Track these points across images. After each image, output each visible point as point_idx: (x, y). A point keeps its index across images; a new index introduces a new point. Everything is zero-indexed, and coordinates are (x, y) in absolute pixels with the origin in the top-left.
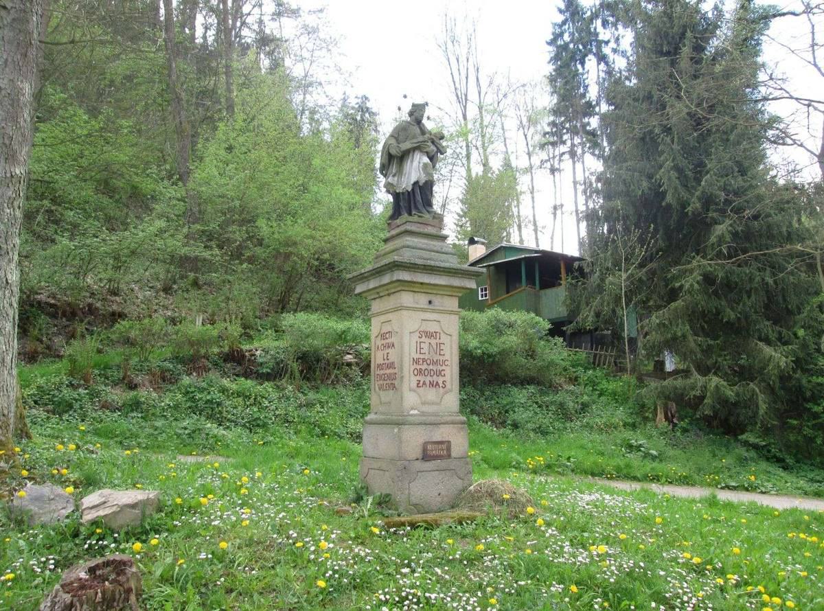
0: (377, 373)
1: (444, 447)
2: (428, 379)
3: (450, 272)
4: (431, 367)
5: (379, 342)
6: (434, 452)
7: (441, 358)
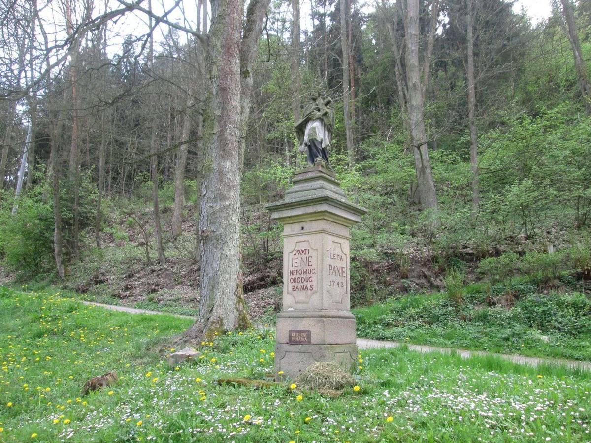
3: (303, 204)
4: (302, 276)
6: (297, 338)
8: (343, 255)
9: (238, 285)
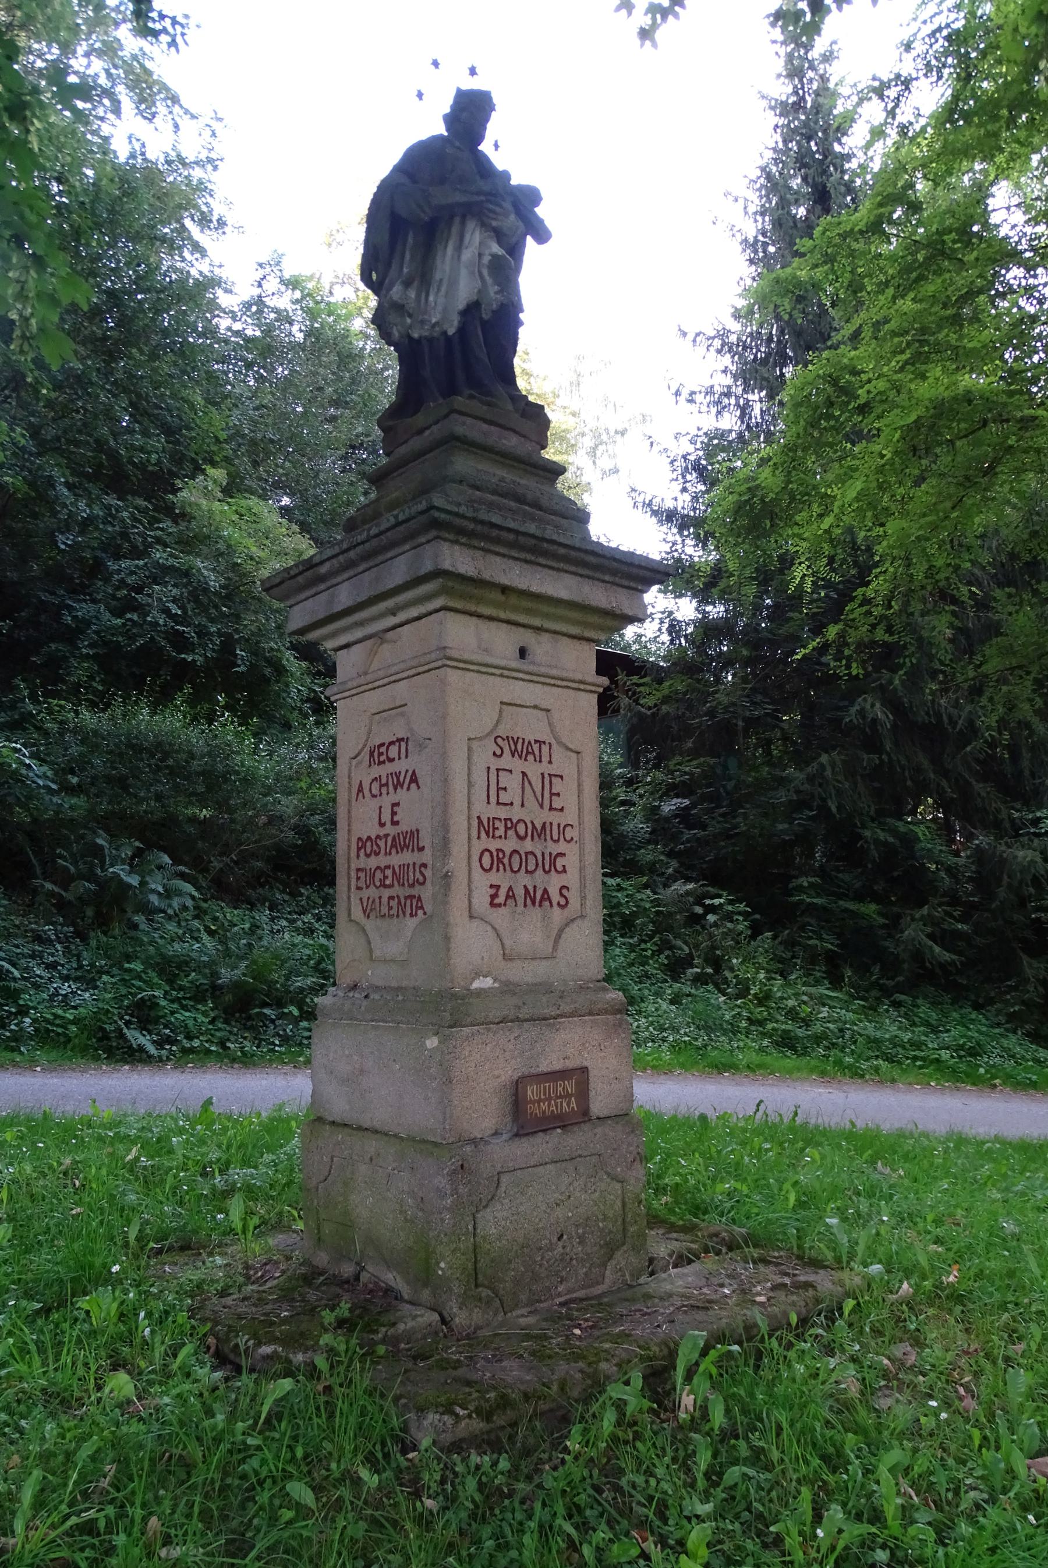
0: (363, 862)
1: (570, 1086)
4: (528, 845)
5: (365, 775)
6: (544, 1106)
7: (555, 818)
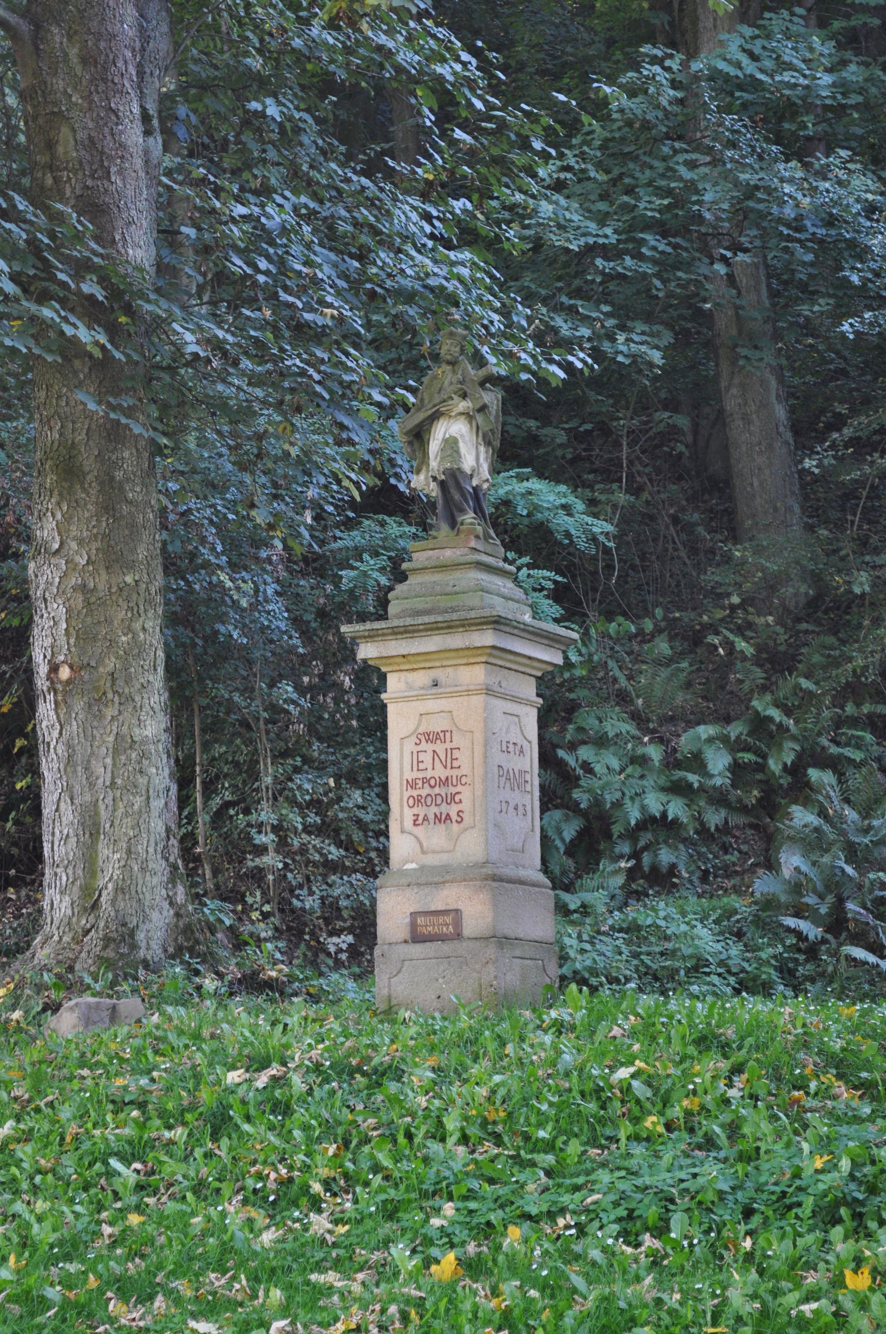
2: (434, 809)
3: (438, 629)
4: (437, 790)
6: (430, 929)
7: (455, 773)
8: (525, 743)
9: (168, 830)
